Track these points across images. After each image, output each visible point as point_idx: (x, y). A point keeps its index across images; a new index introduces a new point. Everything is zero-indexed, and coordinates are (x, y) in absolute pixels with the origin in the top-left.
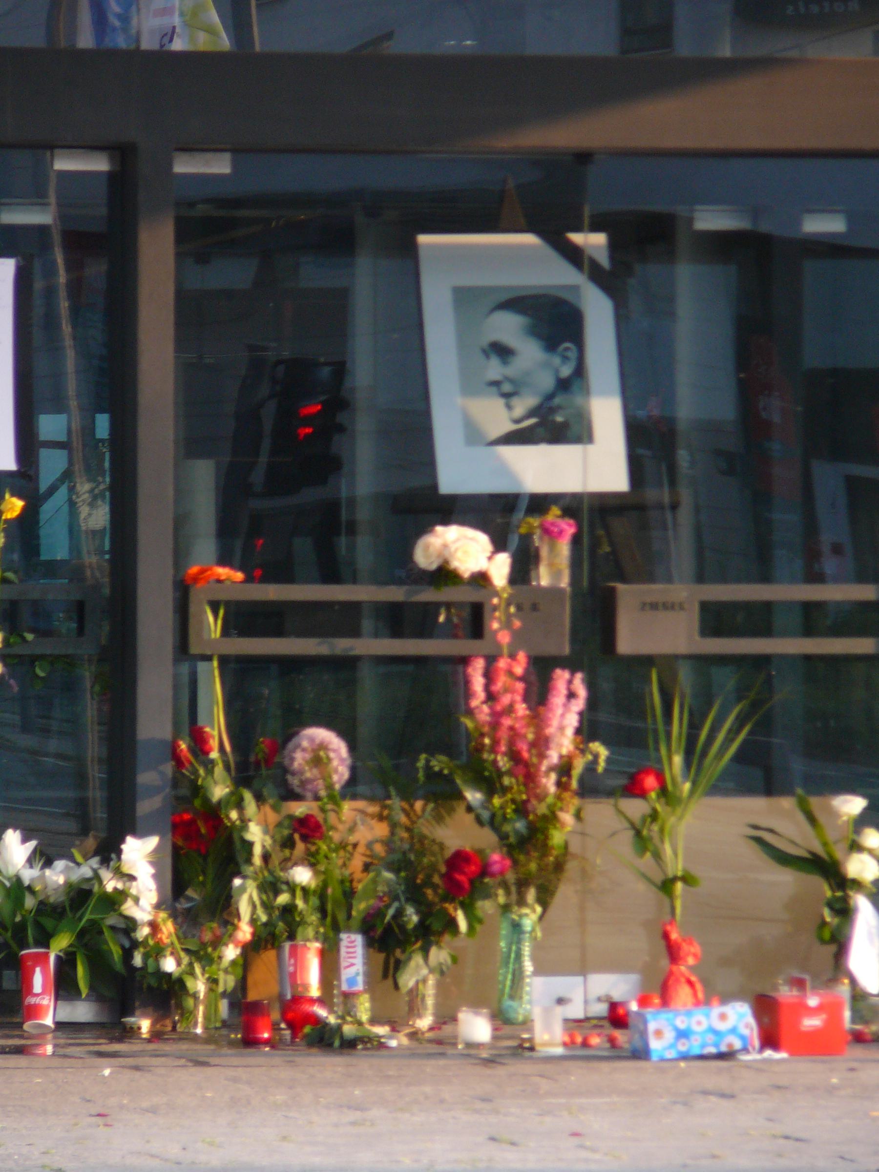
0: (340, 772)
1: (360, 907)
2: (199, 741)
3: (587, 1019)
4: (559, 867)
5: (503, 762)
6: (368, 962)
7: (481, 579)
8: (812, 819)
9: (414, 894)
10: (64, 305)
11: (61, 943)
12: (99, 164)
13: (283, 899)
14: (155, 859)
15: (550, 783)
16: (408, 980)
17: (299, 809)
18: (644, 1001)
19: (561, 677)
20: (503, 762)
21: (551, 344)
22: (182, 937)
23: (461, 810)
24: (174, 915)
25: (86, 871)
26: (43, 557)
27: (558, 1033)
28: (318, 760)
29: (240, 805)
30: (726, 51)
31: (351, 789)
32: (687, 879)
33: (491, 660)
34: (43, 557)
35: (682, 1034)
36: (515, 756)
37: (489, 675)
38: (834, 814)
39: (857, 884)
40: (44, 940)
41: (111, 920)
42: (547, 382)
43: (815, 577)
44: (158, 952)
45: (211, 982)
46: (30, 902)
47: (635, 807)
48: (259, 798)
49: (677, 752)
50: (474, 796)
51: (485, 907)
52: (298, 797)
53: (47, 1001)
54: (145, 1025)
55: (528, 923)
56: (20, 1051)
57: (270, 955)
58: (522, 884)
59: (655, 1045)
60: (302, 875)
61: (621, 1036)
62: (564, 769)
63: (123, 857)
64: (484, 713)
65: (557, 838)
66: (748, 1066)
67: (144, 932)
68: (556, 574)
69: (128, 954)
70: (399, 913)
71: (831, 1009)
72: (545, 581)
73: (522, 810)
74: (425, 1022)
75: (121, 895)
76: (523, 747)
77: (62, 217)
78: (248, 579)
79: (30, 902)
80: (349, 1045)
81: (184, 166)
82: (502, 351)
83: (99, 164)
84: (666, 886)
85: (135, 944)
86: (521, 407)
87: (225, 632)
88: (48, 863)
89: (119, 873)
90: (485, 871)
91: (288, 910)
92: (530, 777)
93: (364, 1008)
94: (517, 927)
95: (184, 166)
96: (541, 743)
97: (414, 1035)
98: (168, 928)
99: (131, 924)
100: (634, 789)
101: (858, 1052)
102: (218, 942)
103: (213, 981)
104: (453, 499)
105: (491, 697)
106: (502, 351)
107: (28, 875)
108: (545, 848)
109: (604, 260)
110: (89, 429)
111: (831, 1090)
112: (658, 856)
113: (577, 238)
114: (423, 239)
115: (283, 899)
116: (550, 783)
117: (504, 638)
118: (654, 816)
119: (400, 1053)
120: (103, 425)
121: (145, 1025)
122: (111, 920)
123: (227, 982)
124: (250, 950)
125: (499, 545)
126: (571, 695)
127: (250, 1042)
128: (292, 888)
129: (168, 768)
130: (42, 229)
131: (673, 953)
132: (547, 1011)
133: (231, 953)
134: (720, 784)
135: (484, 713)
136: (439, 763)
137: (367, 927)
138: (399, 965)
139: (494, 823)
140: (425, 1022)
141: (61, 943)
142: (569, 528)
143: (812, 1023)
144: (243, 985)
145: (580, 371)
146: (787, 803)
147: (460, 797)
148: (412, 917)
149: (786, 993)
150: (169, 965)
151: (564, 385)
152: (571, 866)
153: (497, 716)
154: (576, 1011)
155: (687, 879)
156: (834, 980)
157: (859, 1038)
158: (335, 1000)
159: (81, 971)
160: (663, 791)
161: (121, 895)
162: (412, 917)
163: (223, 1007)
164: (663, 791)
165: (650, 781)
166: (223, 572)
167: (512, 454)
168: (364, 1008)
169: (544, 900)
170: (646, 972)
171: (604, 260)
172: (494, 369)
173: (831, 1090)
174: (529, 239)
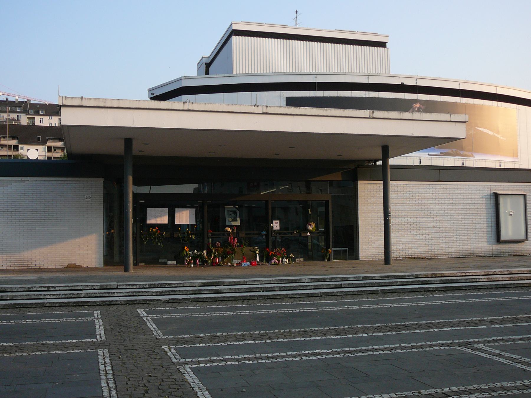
0: (219, 246)
2: (209, 243)
4: (235, 252)
5: (231, 245)
6: (222, 259)
7: (230, 231)
8: (254, 249)
9: (225, 254)
10: (199, 212)
12: (202, 202)
13: (215, 255)
14: (206, 252)
16: (224, 261)
17: (216, 248)
18: (242, 262)
19: (235, 238)
20: (231, 245)
21: (234, 214)
22: (208, 258)
23: (228, 248)
24: (207, 256)
25: (201, 253)
26: (124, 154)
27: (235, 264)
29: (212, 248)
30: (247, 193)
32: (245, 253)
34: (124, 154)
35: (244, 264)
36: (232, 244)
37: (230, 238)
38: (255, 248)
39: (257, 253)
41: (203, 256)
42: (234, 217)
43: (253, 231)
44: (206, 259)
45: (14, 150)
46: (197, 255)
47: (241, 248)
48: (214, 248)
49: (238, 218)
50: (229, 247)
51: (230, 255)
54: (205, 264)
55: (233, 256)
56: (196, 266)
57: (214, 259)
58: (233, 254)
59: (242, 265)
61: (240, 265)
62: (236, 245)
64: (230, 241)
66: (250, 267)
67: (205, 257)
68: (235, 231)
69: (204, 259)
70: (224, 256)
71: (255, 262)
74: (226, 264)
75: (203, 255)
76: (233, 244)
77: (199, 205)
79: (197, 255)
81: (208, 202)
82: (231, 215)
83: (202, 202)
85: (205, 258)
88: (198, 252)
90: (230, 253)
91: (216, 255)
92: (233, 246)
95: (208, 202)
96: (234, 243)
97: (225, 265)
100: (241, 247)
101: (257, 265)
102: (211, 258)
103: (210, 261)
105: (230, 240)
106: (231, 215)
107: (197, 253)
108: (234, 251)
110: (201, 220)
111: (255, 268)
112: (243, 251)
114: (225, 207)
115: (215, 255)
119: (224, 266)
120: (202, 220)
121: (205, 264)
122: (203, 256)
125: (231, 229)
126: (236, 240)
127: (213, 265)
128: (216, 254)
129: (207, 245)
130: (197, 206)
132: (235, 263)
137: (221, 257)
138: (224, 260)
139: (231, 249)
142: (236, 228)
144: (212, 261)
145: (237, 216)
146: (252, 247)
147: (228, 247)
149: (252, 261)
150: (207, 260)
151: (235, 217)
152: (236, 252)
153: (231, 241)
156: (255, 260)
157: (257, 264)
158: (19, 124)
159: (201, 260)
160: (243, 247)
161: (203, 255)
162: (225, 256)
163: (211, 263)
164: (243, 247)
165: (242, 246)
167: (231, 222)
169: (234, 255)
170: (242, 260)
173: (255, 268)
174: (233, 207)
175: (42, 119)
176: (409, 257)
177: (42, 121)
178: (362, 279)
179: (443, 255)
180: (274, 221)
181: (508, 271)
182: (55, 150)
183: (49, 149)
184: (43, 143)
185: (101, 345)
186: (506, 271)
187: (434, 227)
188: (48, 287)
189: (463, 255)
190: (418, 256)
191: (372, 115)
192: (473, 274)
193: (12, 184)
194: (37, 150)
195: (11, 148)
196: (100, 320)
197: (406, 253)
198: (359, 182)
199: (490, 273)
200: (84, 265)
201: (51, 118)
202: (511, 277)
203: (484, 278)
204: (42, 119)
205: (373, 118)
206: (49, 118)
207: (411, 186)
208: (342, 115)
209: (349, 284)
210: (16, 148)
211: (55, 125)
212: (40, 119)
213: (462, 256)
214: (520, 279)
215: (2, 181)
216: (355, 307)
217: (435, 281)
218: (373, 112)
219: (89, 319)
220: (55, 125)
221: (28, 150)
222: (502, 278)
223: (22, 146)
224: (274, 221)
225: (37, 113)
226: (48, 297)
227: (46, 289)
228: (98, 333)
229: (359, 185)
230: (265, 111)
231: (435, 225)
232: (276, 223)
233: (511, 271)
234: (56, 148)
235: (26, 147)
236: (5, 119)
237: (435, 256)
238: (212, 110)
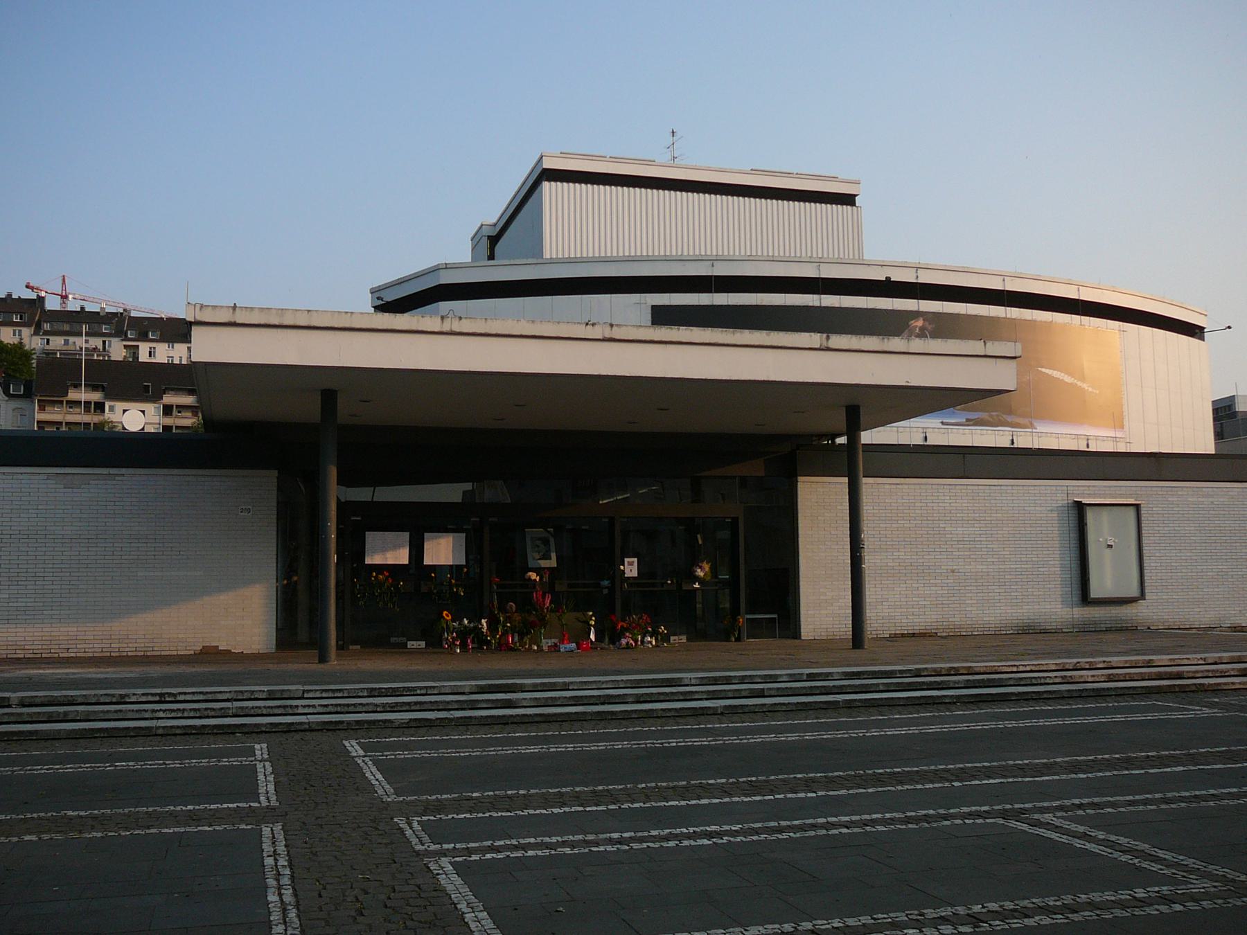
0: (514, 609)
1: (517, 629)
2: (493, 605)
3: (288, 663)
4: (547, 623)
7: (535, 580)
11: (472, 635)
15: (545, 610)
17: (508, 615)
19: (547, 595)
28: (511, 607)
31: (516, 612)
33: (536, 592)
38: (588, 615)
40: (470, 635)
47: (558, 614)
48: (502, 613)
50: (534, 613)
52: (508, 613)
53: (470, 644)
54: (485, 647)
60: (509, 625)
63: (917, 339)
64: (535, 600)
65: (546, 619)
71: (587, 644)
72: (544, 580)
73: (541, 614)
74: (527, 647)
78: (501, 580)
79: (468, 629)
80: (516, 650)
81: (490, 519)
82: (538, 546)
83: (478, 519)
84: (563, 625)
86: (541, 554)
87: (497, 588)
89: (481, 624)
93: (518, 644)
94: (541, 632)
96: (545, 605)
98: (488, 633)
99: (483, 632)
100: (558, 611)
102: (496, 635)
104: (531, 568)
106: (538, 546)
107: (468, 625)
109: (552, 532)
113: (549, 530)
114: (526, 530)
116: (545, 610)
117: (539, 589)
118: (561, 615)
121: (485, 647)
123: (497, 641)
124: (500, 636)
127: (501, 650)
131: (564, 636)
133: (498, 636)
134: (1230, 403)
135: (535, 600)
136: (529, 607)
140: (527, 647)
141: (472, 635)
143: (584, 646)
145: (549, 549)
148: (525, 631)
149: (581, 642)
154: (550, 644)
155: (566, 624)
162: (525, 631)
166: (497, 579)
167: (539, 561)
168: (518, 644)
169: (545, 628)
171: (552, 532)
172: (536, 549)
175: (154, 348)
176: (903, 632)
177: (154, 352)
178: (805, 678)
179: (972, 630)
180: (626, 560)
181: (1104, 662)
182: (179, 412)
183: (168, 410)
184: (155, 398)
185: (268, 815)
186: (1100, 662)
187: (953, 571)
188: (161, 695)
189: (1014, 629)
190: (921, 631)
191: (825, 344)
192: (1034, 668)
193: (91, 482)
194: (143, 412)
195: (90, 408)
196: (267, 764)
197: (897, 625)
198: (800, 479)
199: (1067, 667)
200: (235, 649)
201: (173, 347)
202: (1110, 675)
203: (1056, 677)
204: (154, 348)
205: (829, 349)
206: (169, 347)
207: (906, 487)
208: (765, 344)
209: (778, 689)
210: (100, 407)
211: (181, 360)
212: (150, 348)
213: (1011, 632)
214: (1127, 678)
215: (69, 477)
216: (792, 737)
217: (955, 682)
218: (828, 338)
219: (245, 761)
220: (181, 360)
221: (124, 411)
222: (1093, 676)
223: (112, 403)
224: (626, 560)
225: (143, 337)
226: (161, 714)
227: (157, 698)
228: (262, 790)
229: (800, 485)
230: (607, 335)
231: (955, 567)
232: (631, 564)
233: (1110, 662)
234: (181, 408)
235: (120, 406)
236: (78, 348)
237: (956, 630)
238: (499, 332)
